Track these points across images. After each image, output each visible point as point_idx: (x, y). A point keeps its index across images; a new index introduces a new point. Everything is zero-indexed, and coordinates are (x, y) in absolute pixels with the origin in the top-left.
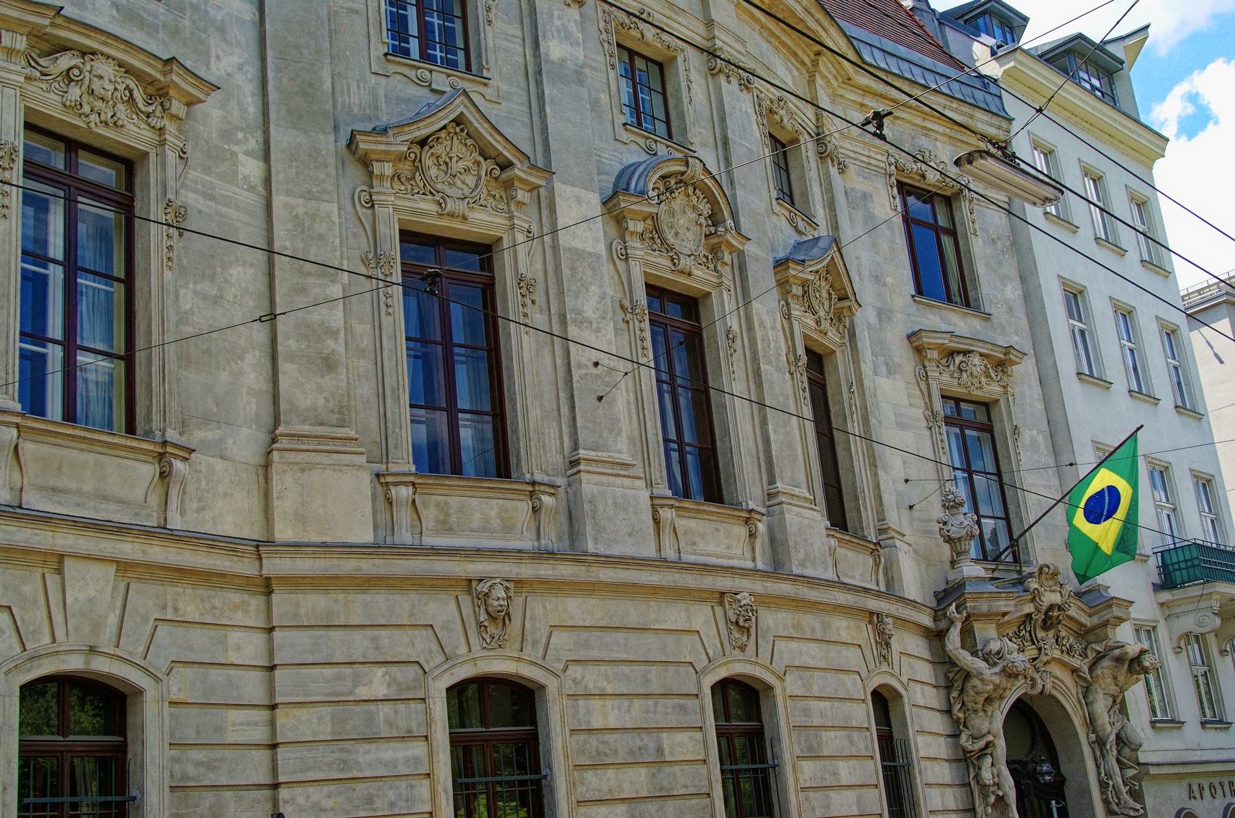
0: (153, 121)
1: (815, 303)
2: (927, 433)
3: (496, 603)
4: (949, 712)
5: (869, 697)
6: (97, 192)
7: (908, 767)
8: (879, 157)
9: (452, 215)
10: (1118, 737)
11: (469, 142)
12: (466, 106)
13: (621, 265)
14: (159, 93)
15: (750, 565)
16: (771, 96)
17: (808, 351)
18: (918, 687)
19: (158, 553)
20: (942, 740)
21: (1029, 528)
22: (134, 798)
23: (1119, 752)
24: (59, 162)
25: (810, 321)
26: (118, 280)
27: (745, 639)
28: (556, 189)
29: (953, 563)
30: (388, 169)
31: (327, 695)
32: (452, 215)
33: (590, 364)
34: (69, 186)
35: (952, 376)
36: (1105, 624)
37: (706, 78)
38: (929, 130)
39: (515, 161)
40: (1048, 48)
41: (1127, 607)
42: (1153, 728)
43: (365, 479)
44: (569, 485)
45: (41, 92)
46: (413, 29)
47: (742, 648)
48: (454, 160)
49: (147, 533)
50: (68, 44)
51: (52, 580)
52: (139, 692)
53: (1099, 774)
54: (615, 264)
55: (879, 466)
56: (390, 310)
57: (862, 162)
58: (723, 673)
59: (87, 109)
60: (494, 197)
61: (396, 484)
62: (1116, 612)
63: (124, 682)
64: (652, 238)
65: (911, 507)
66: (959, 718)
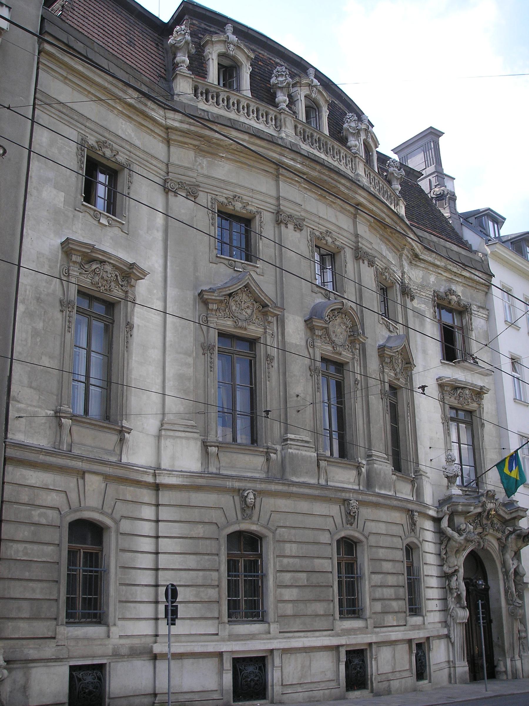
0: (124, 288)
1: (395, 365)
2: (442, 425)
3: (250, 500)
4: (440, 555)
5: (404, 548)
6: (99, 318)
7: (419, 580)
9: (241, 328)
10: (515, 570)
11: (250, 295)
12: (250, 280)
13: (311, 350)
15: (357, 487)
20: (435, 567)
21: (485, 473)
23: (515, 577)
27: (352, 520)
28: (285, 315)
29: (448, 487)
30: (215, 307)
32: (241, 328)
33: (295, 395)
34: (90, 316)
35: (455, 399)
36: (514, 518)
37: (354, 262)
39: (269, 304)
40: (513, 236)
41: (526, 511)
44: (283, 449)
45: (84, 278)
47: (351, 524)
48: (243, 303)
51: (81, 481)
52: (108, 528)
53: (505, 586)
54: (308, 350)
56: (212, 369)
58: (343, 534)
59: (100, 285)
60: (259, 319)
61: (211, 446)
62: (521, 514)
64: (325, 338)
65: (431, 460)
66: (444, 558)
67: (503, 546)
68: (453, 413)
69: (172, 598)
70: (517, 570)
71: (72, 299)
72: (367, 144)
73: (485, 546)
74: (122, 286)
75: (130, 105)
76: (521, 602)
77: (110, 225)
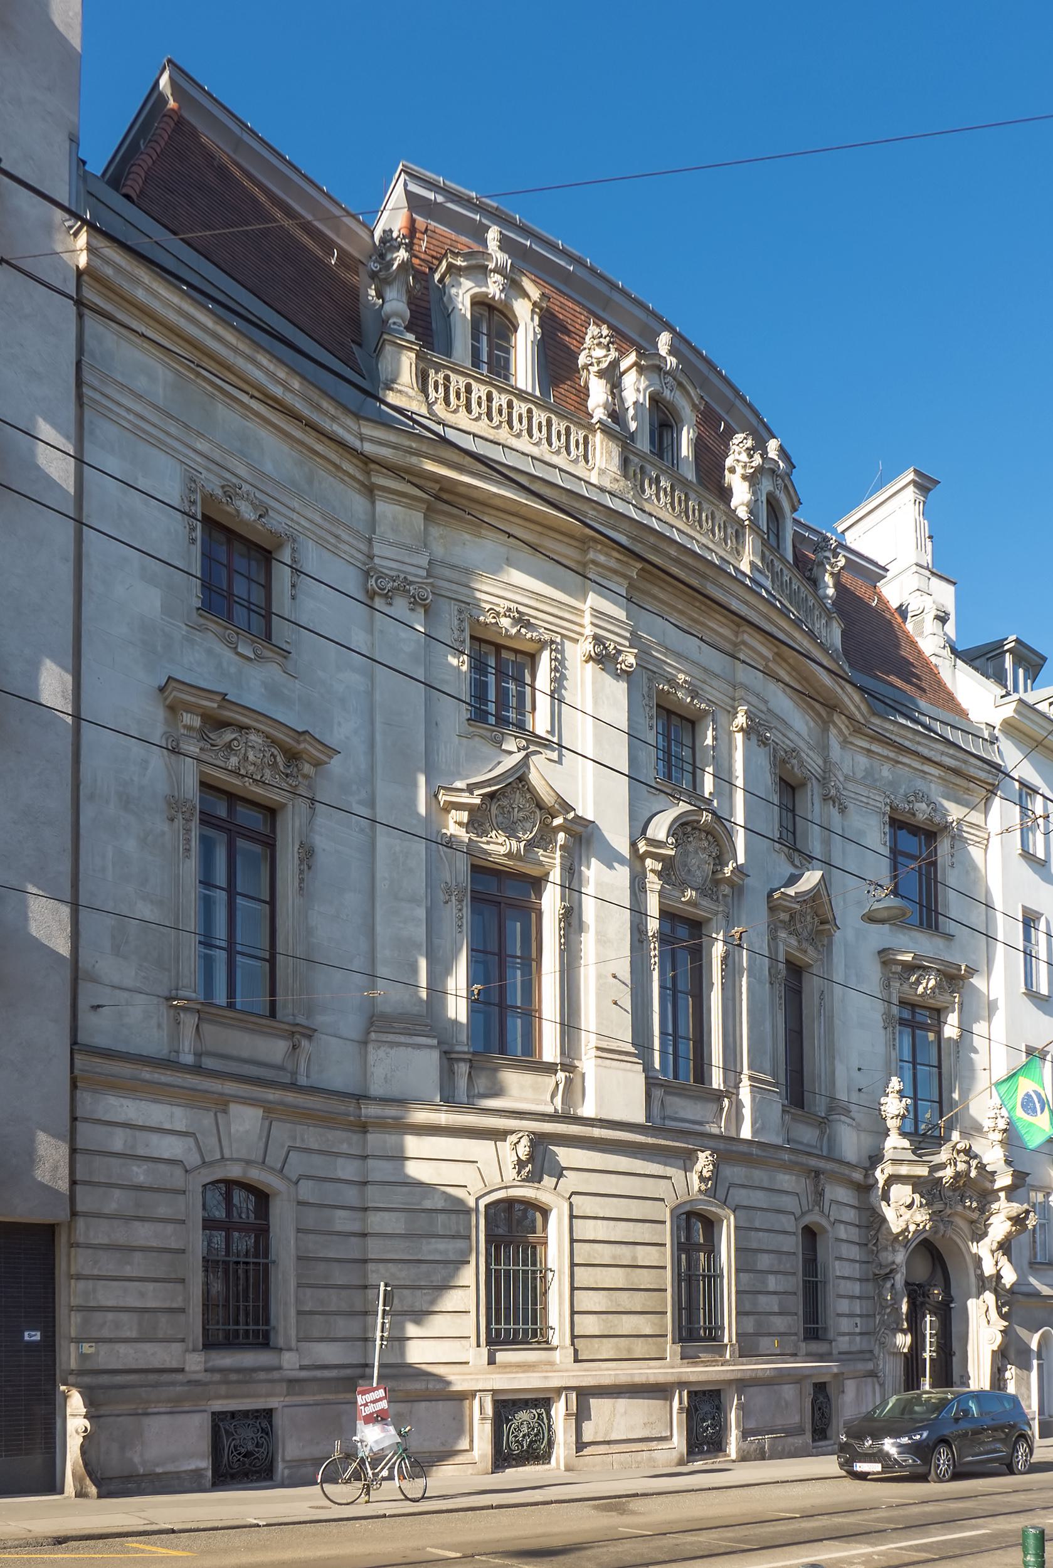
6: (251, 836)
8: (877, 798)
14: (293, 757)
16: (785, 747)
17: (788, 962)
18: (842, 1226)
19: (290, 1097)
22: (274, 1262)
24: (222, 812)
25: (793, 941)
26: (265, 902)
31: (403, 1204)
38: (925, 773)
42: (1031, 1268)
43: (435, 1055)
46: (492, 696)
48: (516, 810)
49: (284, 1087)
50: (232, 721)
55: (837, 1058)
57: (861, 801)
63: (269, 1185)
68: (906, 1015)
71: (190, 796)
72: (774, 503)
74: (287, 775)
75: (949, 769)
77: (259, 657)
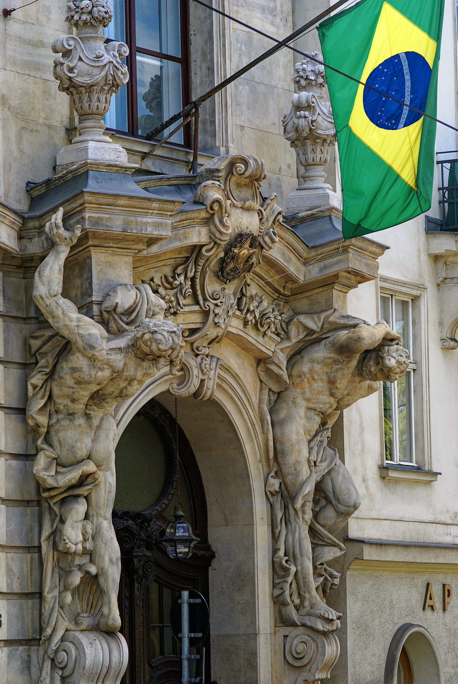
41: (375, 256)
53: (275, 551)
65: (7, 13)
66: (38, 426)
67: (276, 388)
69: (191, 631)
70: (329, 485)
73: (210, 384)
76: (333, 614)
